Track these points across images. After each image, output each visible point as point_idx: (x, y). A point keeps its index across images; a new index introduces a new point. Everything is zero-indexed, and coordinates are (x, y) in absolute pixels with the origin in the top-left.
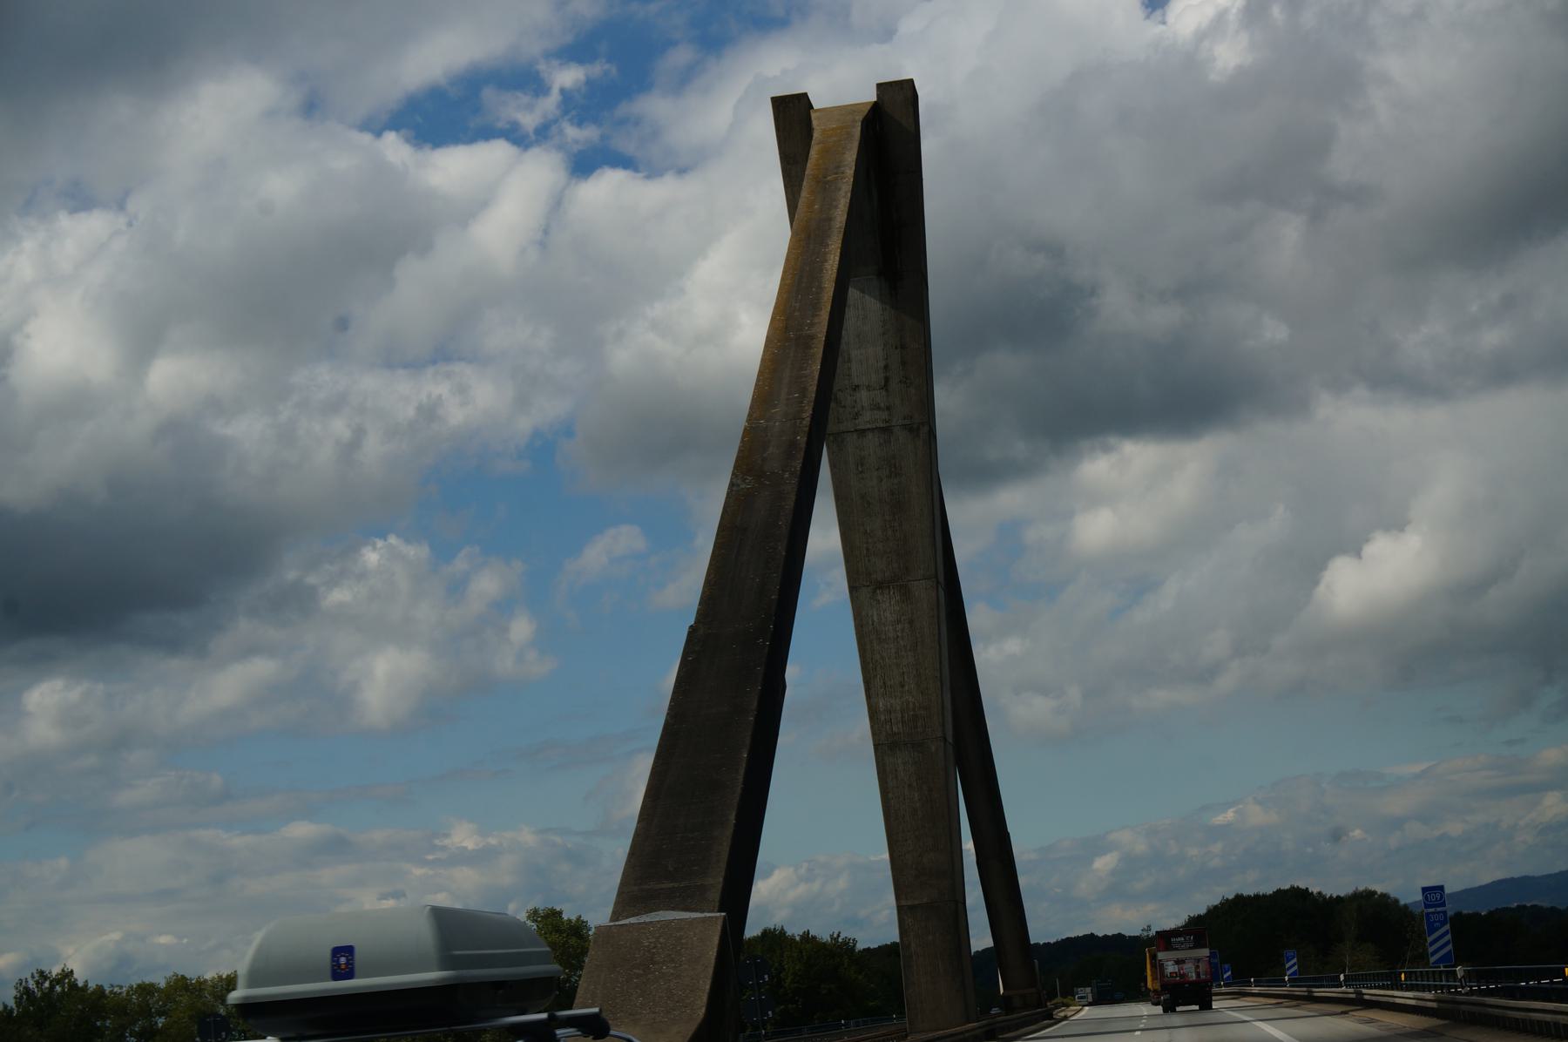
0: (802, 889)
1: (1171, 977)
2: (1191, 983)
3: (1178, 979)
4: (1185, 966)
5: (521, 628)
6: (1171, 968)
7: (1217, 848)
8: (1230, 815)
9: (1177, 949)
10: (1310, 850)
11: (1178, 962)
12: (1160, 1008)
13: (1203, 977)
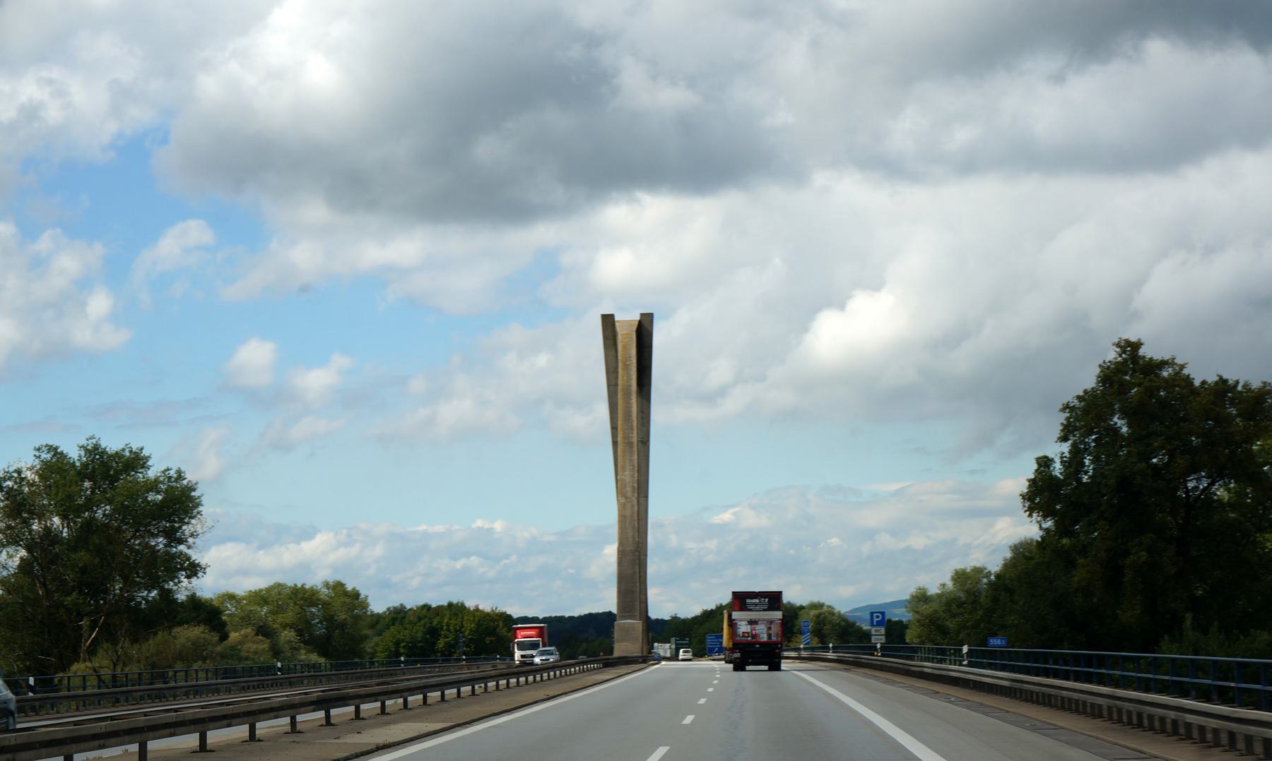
0: (342, 552)
1: (743, 636)
2: (763, 644)
3: (749, 639)
4: (757, 627)
5: (99, 304)
6: (743, 628)
7: (712, 544)
8: (727, 516)
9: (750, 610)
10: (792, 552)
11: (751, 622)
12: (732, 665)
13: (774, 638)
